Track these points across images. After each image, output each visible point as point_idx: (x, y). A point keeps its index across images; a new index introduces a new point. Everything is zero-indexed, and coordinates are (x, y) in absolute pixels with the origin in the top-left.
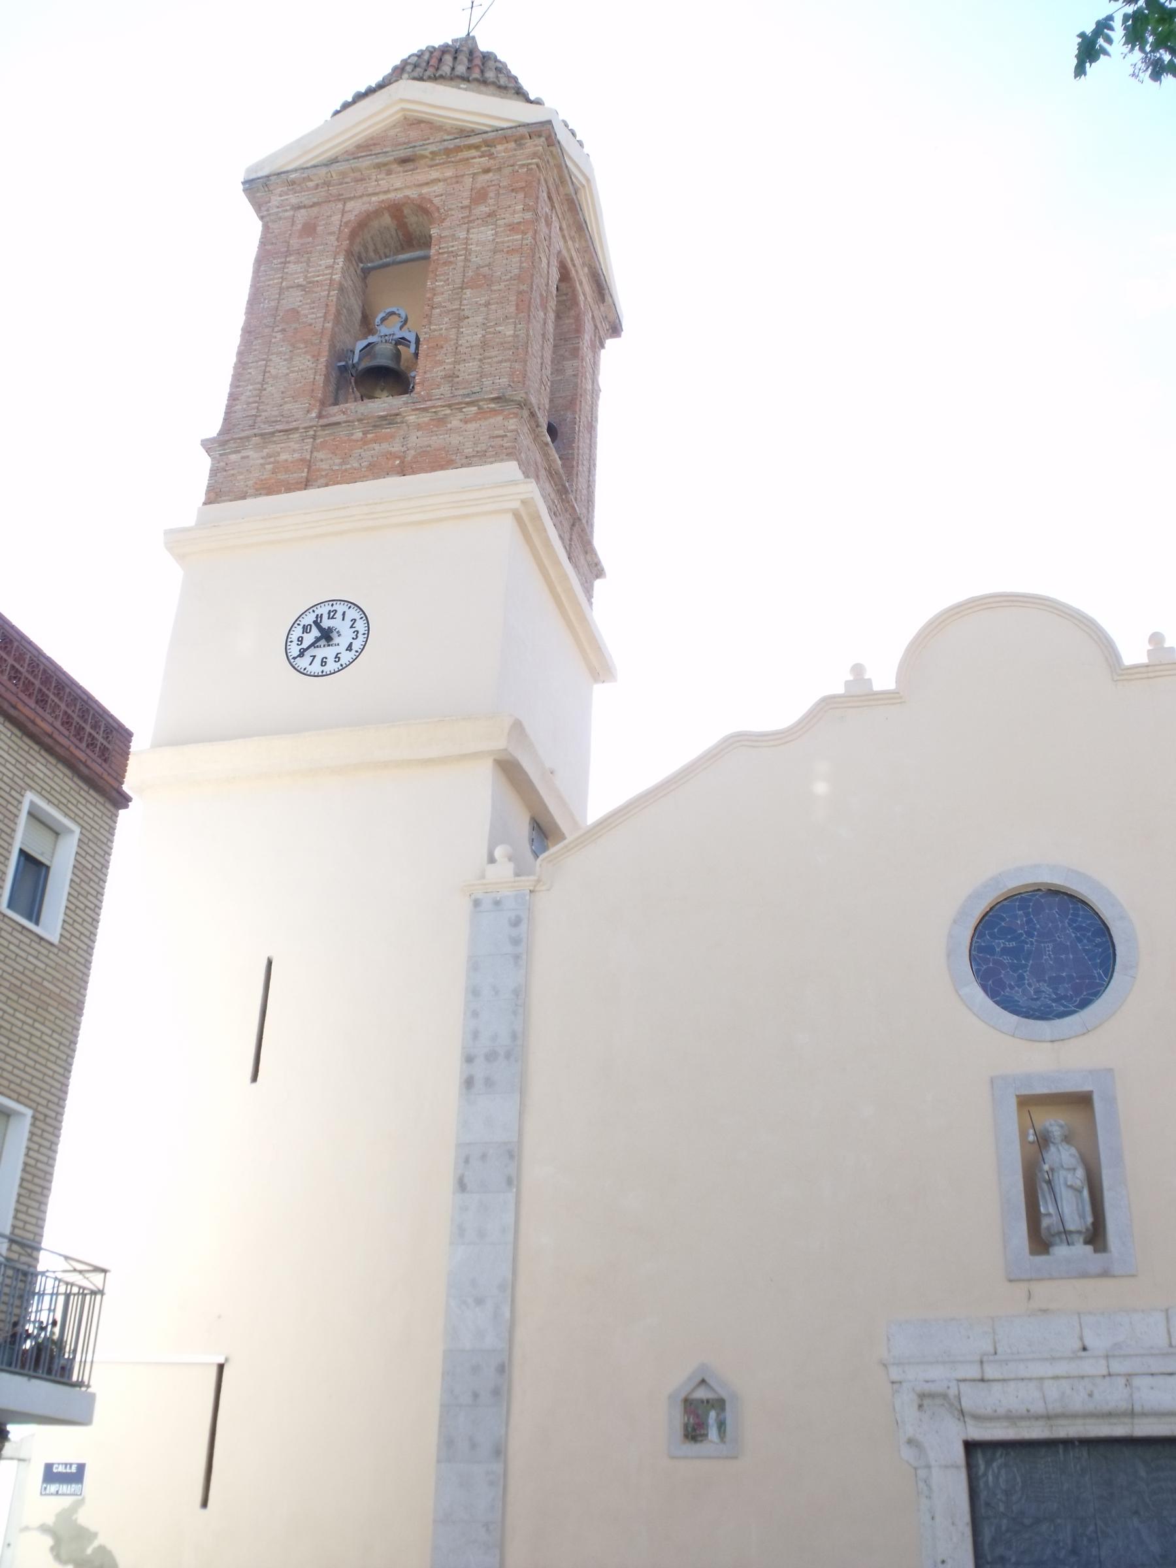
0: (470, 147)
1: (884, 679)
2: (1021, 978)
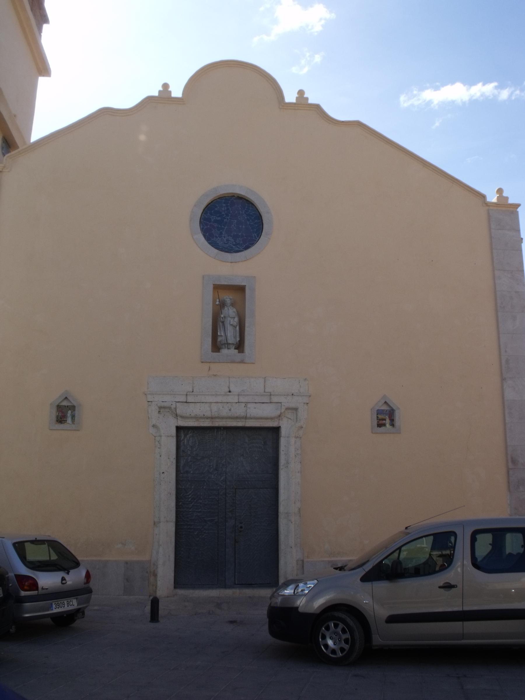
1: (177, 92)
2: (221, 233)
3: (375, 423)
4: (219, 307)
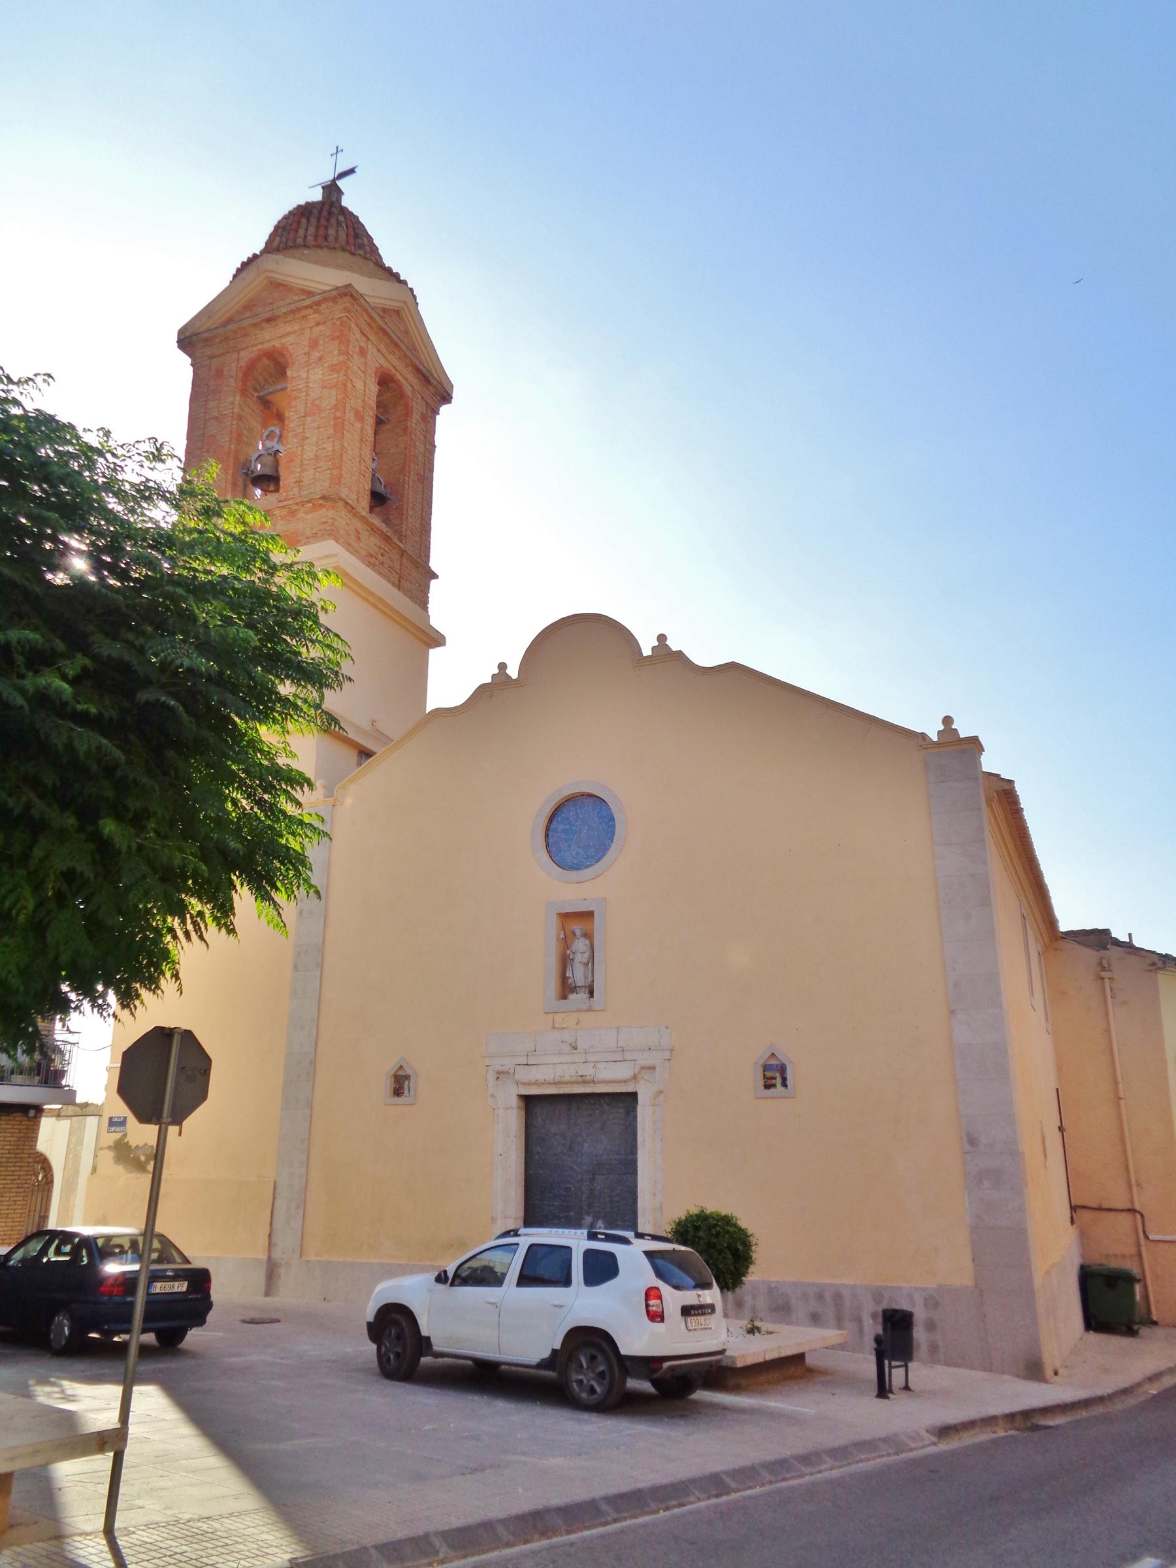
0: (306, 307)
1: (513, 672)
2: (569, 846)
3: (761, 1082)
4: (566, 942)
